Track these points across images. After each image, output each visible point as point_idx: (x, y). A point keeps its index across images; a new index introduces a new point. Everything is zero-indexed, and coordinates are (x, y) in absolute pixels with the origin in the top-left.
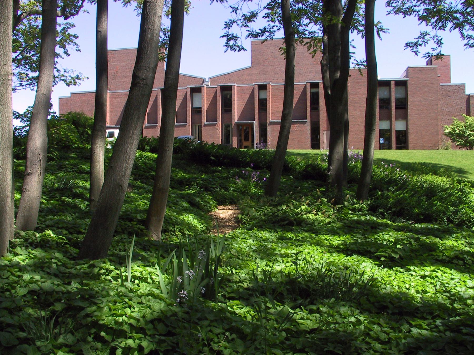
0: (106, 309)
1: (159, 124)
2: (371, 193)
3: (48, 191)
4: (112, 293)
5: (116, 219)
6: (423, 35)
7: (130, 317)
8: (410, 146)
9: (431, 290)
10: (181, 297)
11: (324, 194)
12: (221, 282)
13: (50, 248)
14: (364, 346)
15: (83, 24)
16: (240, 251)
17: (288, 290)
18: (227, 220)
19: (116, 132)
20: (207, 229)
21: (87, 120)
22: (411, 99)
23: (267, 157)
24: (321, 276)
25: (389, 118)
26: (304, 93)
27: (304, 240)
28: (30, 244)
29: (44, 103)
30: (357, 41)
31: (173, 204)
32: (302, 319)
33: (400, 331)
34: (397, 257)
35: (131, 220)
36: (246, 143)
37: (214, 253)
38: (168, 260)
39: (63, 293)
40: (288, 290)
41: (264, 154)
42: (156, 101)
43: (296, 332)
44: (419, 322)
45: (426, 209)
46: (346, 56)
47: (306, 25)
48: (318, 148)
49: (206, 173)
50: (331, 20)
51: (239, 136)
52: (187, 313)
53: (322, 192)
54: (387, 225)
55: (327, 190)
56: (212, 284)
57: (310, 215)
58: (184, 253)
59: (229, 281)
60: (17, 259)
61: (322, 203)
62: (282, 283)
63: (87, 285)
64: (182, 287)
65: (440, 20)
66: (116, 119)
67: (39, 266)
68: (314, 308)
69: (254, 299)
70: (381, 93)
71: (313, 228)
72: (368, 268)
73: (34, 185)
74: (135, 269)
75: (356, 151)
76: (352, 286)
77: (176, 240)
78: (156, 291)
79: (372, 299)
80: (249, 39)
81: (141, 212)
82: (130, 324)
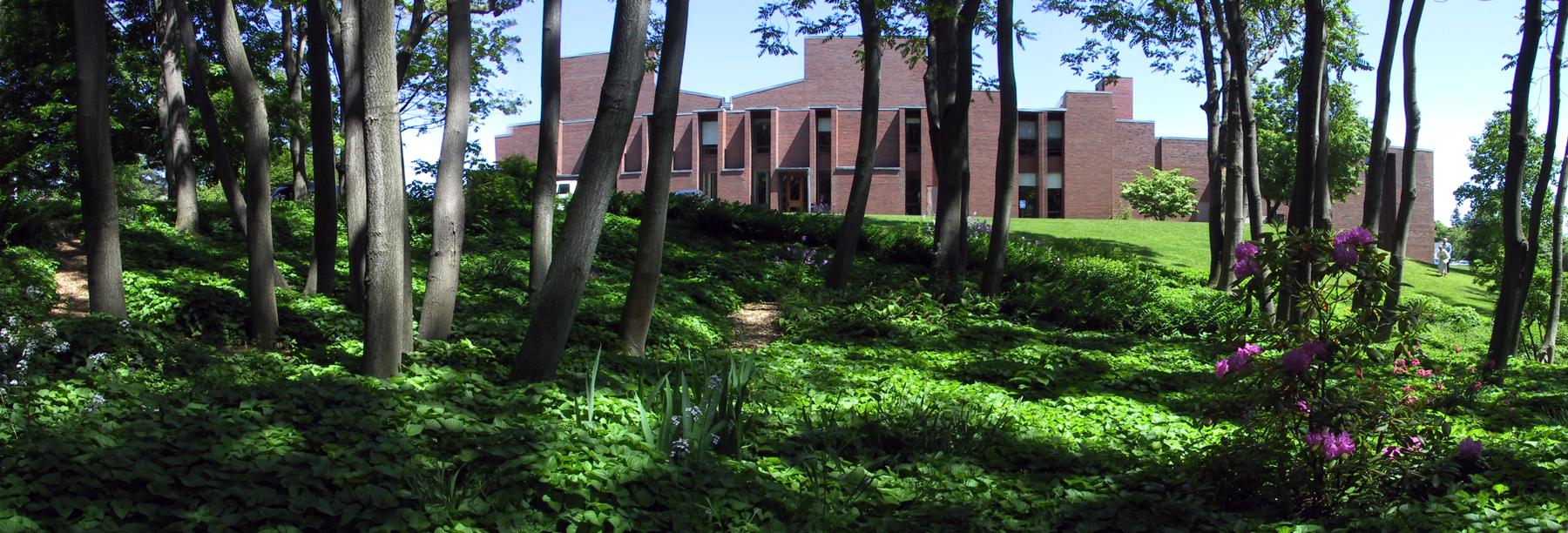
0: (552, 460)
1: (644, 172)
2: (1005, 286)
3: (464, 277)
4: (562, 436)
5: (571, 321)
6: (1090, 45)
7: (591, 476)
8: (1067, 209)
9: (1097, 431)
10: (677, 450)
11: (927, 286)
12: (747, 427)
13: (466, 366)
14: (990, 525)
15: (526, 22)
16: (781, 378)
17: (863, 440)
18: (759, 327)
19: (573, 185)
20: (725, 341)
21: (528, 166)
22: (1068, 140)
23: (831, 226)
24: (920, 416)
25: (1035, 169)
26: (895, 124)
27: (892, 360)
28: (435, 360)
29: (458, 146)
30: (984, 48)
31: (666, 299)
32: (887, 486)
33: (1053, 496)
34: (1046, 382)
35: (595, 323)
36: (793, 204)
37: (736, 379)
38: (656, 389)
39: (479, 434)
40: (863, 440)
41: (826, 221)
42: (639, 136)
43: (878, 508)
44: (1078, 480)
45: (1091, 309)
46: (967, 70)
47: (900, 17)
48: (919, 213)
49: (724, 250)
50: (942, 11)
51: (782, 191)
52: (688, 475)
53: (923, 283)
54: (1030, 335)
55: (932, 280)
56: (732, 431)
57: (902, 320)
58: (683, 377)
59: (762, 425)
60: (411, 381)
61: (923, 300)
62: (853, 428)
63: (523, 420)
64: (679, 432)
65: (1116, 25)
66: (572, 164)
67: (444, 393)
68: (909, 468)
69: (803, 456)
70: (1022, 131)
71: (908, 341)
72: (998, 402)
73: (447, 269)
74: (600, 400)
75: (981, 219)
76: (972, 430)
77: (670, 357)
78: (635, 438)
79: (1004, 450)
80: (802, 36)
81: (611, 310)
82: (591, 487)
